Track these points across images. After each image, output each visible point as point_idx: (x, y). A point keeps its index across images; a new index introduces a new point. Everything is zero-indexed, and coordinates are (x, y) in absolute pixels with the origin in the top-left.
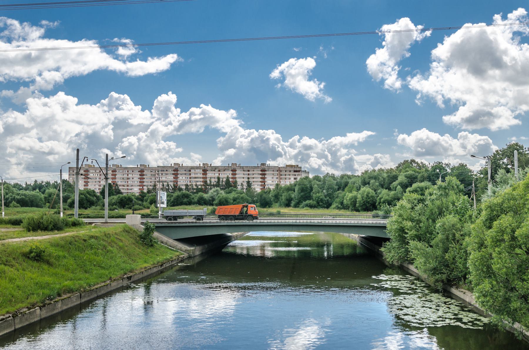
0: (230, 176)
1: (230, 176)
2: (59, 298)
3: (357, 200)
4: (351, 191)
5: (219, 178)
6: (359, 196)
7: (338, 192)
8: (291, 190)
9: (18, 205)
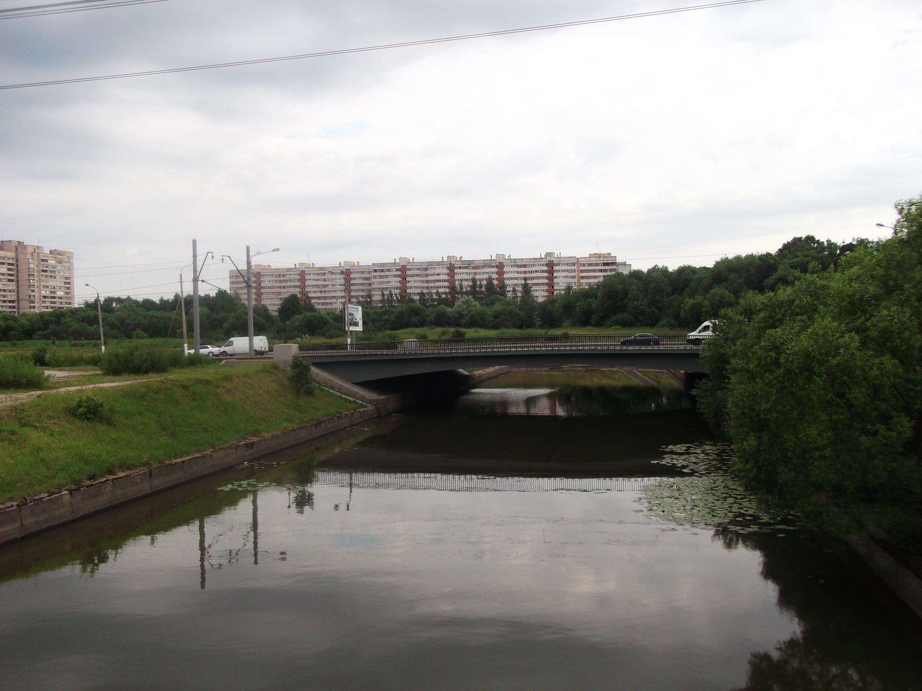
0: (495, 276)
1: (495, 276)
2: (111, 477)
3: (703, 310)
4: (692, 296)
5: (474, 280)
6: (706, 302)
7: (671, 298)
8: (591, 296)
9: (146, 335)
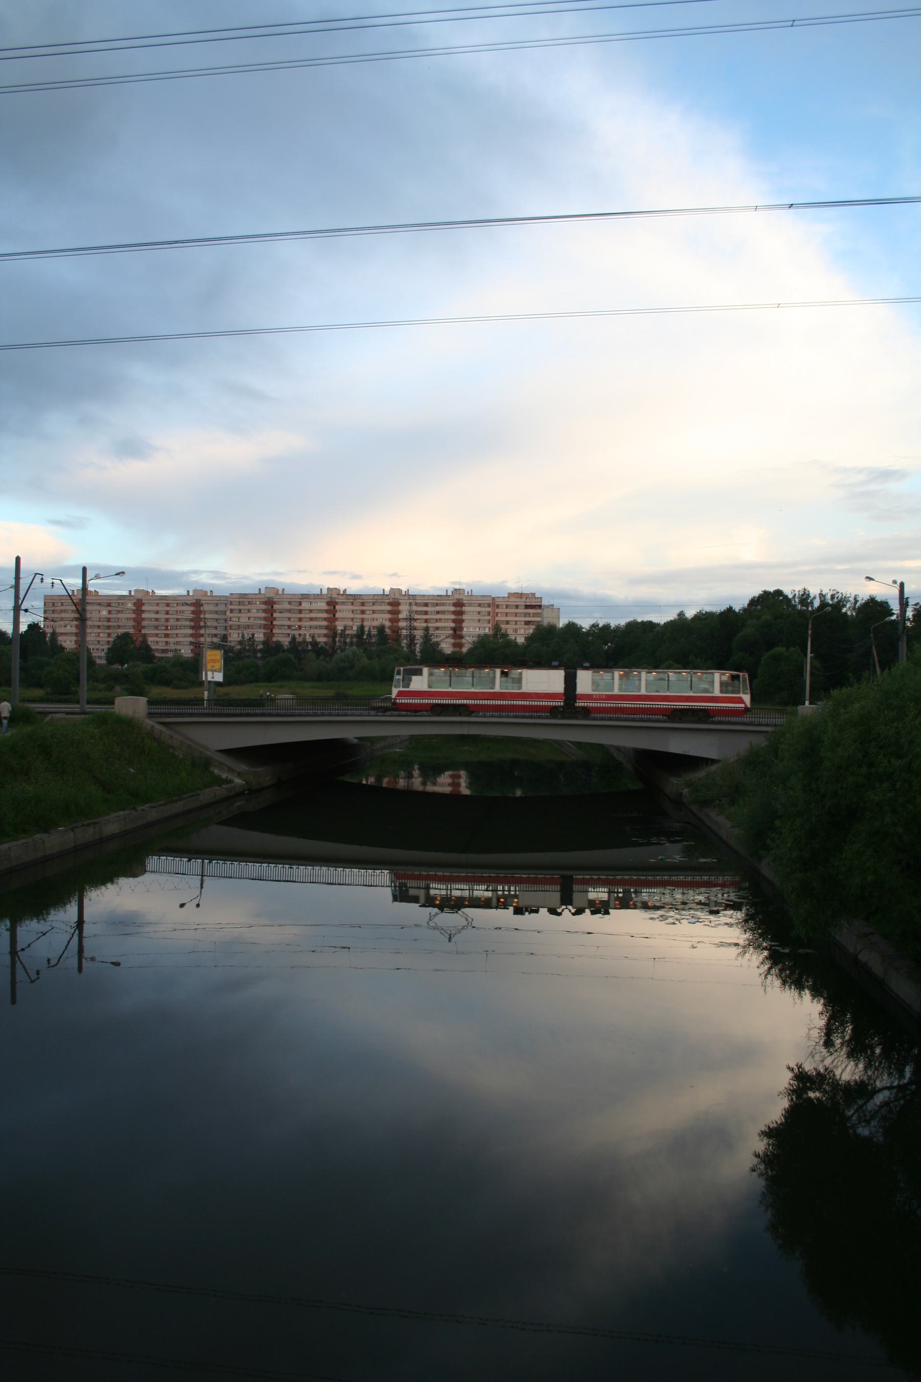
0: (388, 624)
1: (388, 624)
